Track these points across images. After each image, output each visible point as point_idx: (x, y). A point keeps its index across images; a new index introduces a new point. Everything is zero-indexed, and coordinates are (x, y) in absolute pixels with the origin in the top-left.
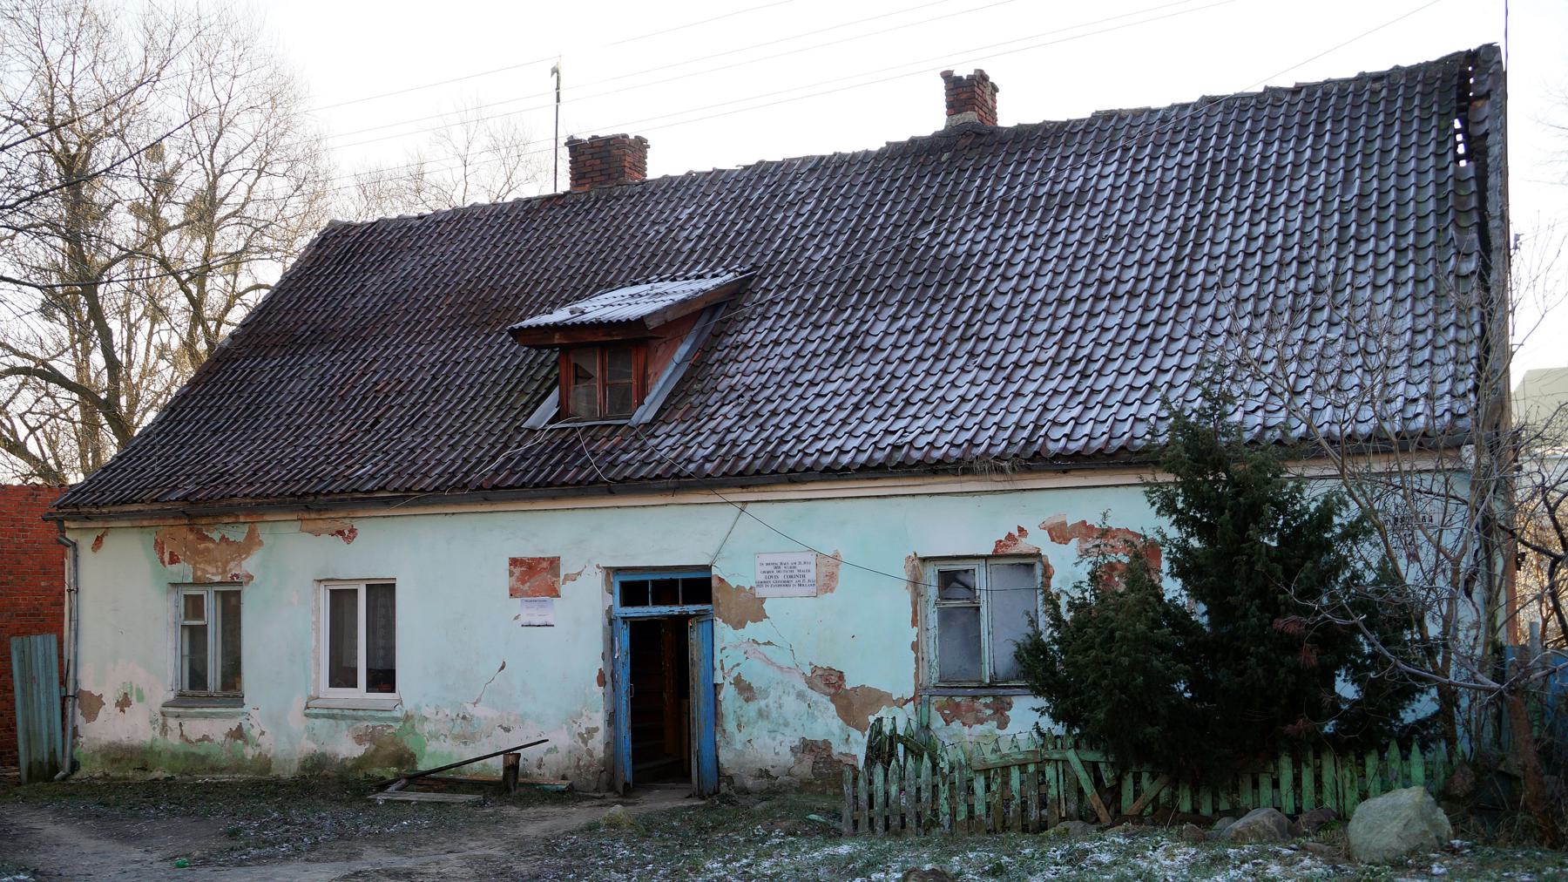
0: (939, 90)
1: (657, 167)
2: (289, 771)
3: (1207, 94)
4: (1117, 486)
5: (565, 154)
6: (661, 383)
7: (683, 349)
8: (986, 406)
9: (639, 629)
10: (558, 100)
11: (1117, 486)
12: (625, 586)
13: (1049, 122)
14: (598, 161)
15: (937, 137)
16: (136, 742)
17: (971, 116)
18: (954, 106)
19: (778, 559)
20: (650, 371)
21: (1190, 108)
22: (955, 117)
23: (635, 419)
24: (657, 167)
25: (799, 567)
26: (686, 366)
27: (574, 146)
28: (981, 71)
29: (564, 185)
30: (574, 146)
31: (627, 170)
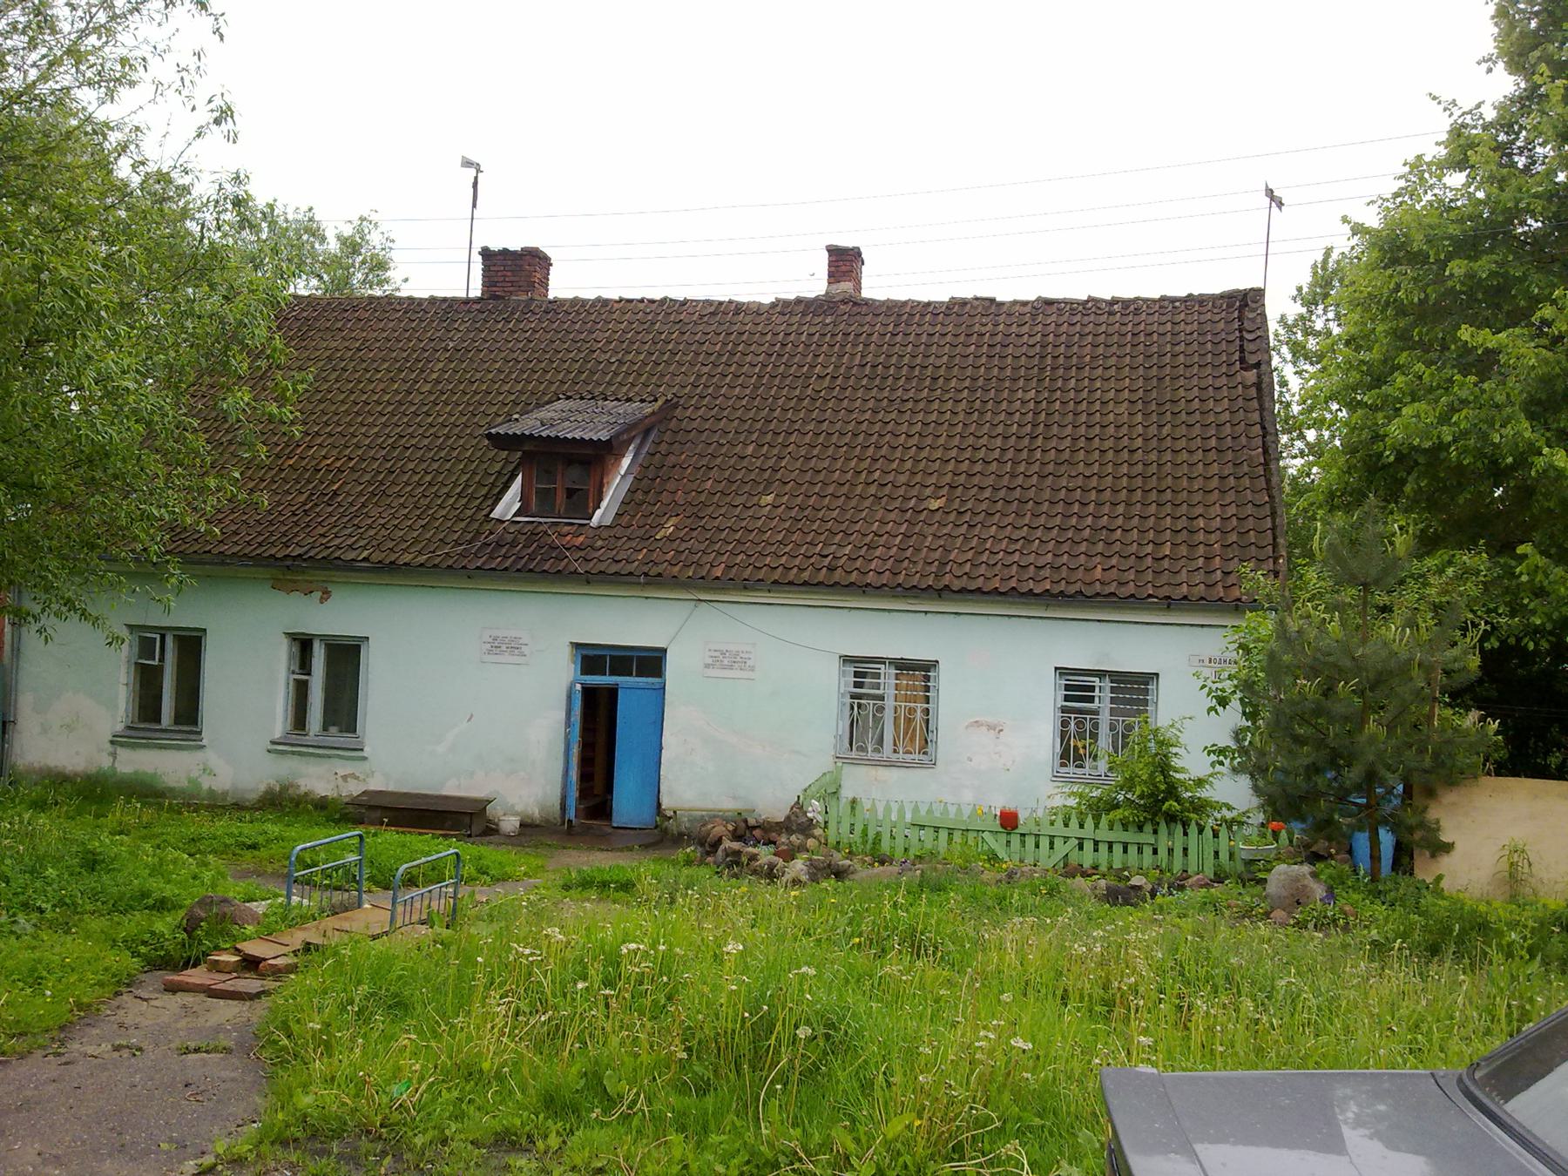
0: (824, 257)
1: (562, 285)
2: (253, 796)
3: (1043, 296)
4: (1202, 626)
5: (478, 261)
6: (611, 493)
7: (626, 462)
8: (363, 500)
9: (589, 694)
10: (474, 206)
11: (1202, 626)
12: (585, 659)
13: (892, 301)
14: (509, 274)
15: (816, 299)
16: (1297, 1151)
17: (846, 286)
18: (835, 275)
19: (723, 648)
20: (605, 481)
21: (1030, 305)
22: (835, 286)
23: (595, 521)
24: (562, 285)
25: (742, 655)
26: (630, 479)
27: (486, 254)
28: (858, 248)
29: (476, 291)
30: (486, 254)
31: (536, 285)
